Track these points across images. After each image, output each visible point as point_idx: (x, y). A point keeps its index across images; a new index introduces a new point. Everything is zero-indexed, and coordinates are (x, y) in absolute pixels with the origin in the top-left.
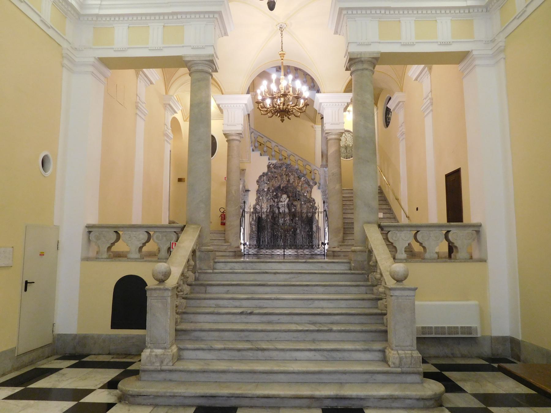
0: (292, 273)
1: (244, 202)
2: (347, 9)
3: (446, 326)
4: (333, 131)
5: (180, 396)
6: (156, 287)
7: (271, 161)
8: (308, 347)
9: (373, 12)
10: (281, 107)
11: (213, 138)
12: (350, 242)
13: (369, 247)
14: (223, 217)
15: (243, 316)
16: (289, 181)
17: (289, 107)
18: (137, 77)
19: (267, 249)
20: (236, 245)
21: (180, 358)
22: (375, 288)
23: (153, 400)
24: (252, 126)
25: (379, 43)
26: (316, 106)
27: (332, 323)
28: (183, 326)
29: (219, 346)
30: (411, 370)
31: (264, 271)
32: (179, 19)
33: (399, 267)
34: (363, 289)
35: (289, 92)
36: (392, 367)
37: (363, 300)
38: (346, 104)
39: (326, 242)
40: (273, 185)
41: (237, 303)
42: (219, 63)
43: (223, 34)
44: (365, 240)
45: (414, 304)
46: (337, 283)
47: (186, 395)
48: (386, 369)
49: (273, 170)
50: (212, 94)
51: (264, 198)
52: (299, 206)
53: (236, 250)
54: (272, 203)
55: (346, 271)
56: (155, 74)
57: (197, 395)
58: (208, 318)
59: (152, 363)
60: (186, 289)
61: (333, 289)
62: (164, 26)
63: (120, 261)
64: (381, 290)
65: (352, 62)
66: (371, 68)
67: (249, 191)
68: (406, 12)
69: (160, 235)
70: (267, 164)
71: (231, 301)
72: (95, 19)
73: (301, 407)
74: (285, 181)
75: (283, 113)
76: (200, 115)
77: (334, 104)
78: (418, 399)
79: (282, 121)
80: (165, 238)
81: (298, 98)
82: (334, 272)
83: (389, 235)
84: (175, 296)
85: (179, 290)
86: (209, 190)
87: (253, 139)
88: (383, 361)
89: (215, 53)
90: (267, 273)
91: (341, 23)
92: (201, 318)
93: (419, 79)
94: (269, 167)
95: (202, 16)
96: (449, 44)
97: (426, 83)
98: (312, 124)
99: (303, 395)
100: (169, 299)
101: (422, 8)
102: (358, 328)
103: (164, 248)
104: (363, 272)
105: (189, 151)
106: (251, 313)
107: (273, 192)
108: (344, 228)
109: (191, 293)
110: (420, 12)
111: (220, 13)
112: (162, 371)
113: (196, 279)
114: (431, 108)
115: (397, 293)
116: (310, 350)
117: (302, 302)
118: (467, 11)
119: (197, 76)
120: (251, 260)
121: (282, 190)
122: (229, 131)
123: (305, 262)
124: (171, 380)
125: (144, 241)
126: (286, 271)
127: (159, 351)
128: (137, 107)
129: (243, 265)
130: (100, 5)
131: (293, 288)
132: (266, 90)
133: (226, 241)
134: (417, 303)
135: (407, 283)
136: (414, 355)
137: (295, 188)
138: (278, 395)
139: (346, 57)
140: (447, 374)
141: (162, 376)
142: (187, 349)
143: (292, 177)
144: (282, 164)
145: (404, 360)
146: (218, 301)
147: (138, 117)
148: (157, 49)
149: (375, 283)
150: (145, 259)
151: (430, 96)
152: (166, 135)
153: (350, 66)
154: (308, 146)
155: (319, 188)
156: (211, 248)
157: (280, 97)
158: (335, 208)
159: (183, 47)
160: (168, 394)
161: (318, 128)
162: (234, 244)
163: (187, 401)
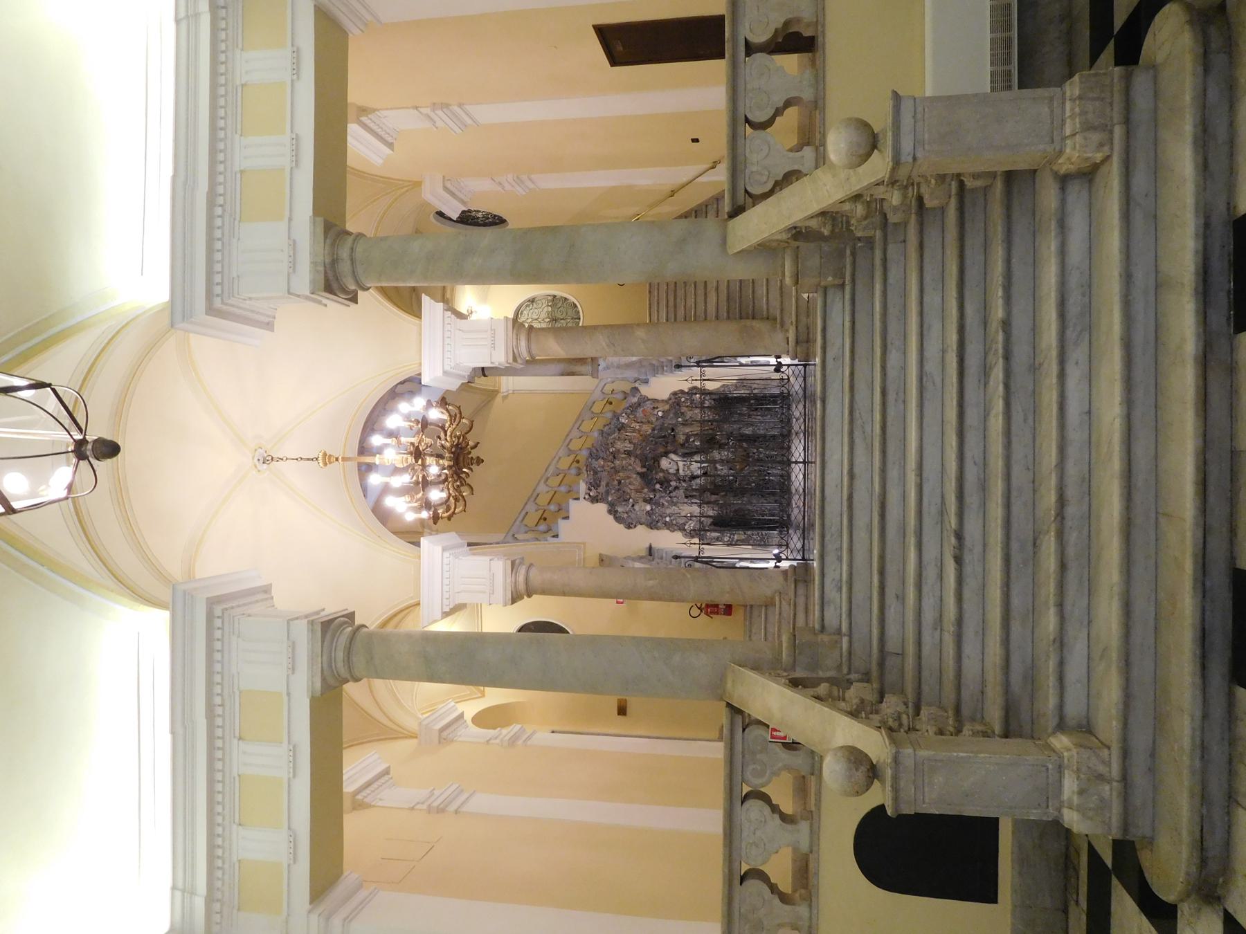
0: (851, 433)
1: (676, 557)
2: (209, 295)
3: (988, 36)
4: (510, 344)
5: (1203, 729)
6: (889, 788)
7: (582, 495)
8: (1054, 381)
9: (218, 234)
10: (446, 463)
11: (523, 629)
12: (775, 303)
13: (784, 236)
14: (711, 609)
15: (967, 558)
16: (629, 453)
17: (448, 445)
18: (369, 806)
19: (789, 504)
20: (781, 579)
21: (1085, 728)
22: (893, 218)
23: (1217, 806)
24: (500, 537)
25: (290, 219)
26: (454, 385)
27: (985, 324)
28: (994, 714)
29: (1050, 621)
30: (1118, 97)
31: (845, 503)
32: (223, 700)
33: (837, 144)
34: (892, 249)
35: (412, 444)
36: (1112, 149)
37: (921, 246)
38: (449, 313)
39: (773, 361)
40: (637, 491)
41: (930, 573)
42: (332, 607)
43: (265, 596)
44: (766, 249)
45: (933, 100)
46: (877, 317)
47: (1198, 714)
48: (1115, 166)
49: (602, 489)
50: (419, 629)
51: (668, 511)
52: (687, 430)
53: (791, 579)
54: (681, 492)
55: (847, 297)
56: (357, 768)
57: (1198, 681)
58: (970, 649)
59: (1103, 805)
60: (892, 705)
61: (893, 327)
62: (240, 739)
63: (817, 874)
64: (895, 198)
65: (335, 286)
66: (350, 239)
67: (650, 548)
68: (221, 157)
69: (751, 767)
70: (588, 504)
71: (925, 589)
72: (217, 907)
73: (1232, 393)
74: (631, 461)
75: (461, 458)
76: (463, 660)
77: (447, 341)
78: (1207, 70)
79: (480, 461)
80: (758, 756)
81: (424, 424)
82: (847, 324)
83: (756, 190)
84: (913, 735)
85: (895, 725)
86: (638, 641)
87: (530, 535)
88: (1091, 181)
89: (306, 617)
90: (850, 497)
91: (245, 313)
92: (971, 668)
93: (390, 139)
94: (594, 500)
95: (218, 645)
96: (297, 53)
97: (398, 120)
98: (499, 399)
99: (1197, 387)
100: (923, 753)
101: (213, 118)
102: (998, 253)
103: (784, 755)
104: (848, 252)
105: (542, 689)
106: (959, 536)
107: (654, 490)
108: (741, 318)
109: (902, 692)
110: (221, 123)
111: (212, 602)
112: (1125, 778)
113: (866, 677)
114: (456, 108)
115: (907, 145)
116: (1062, 375)
117: (926, 404)
118: (223, 13)
119: (359, 661)
120: (817, 538)
121: (650, 469)
122: (505, 590)
123: (824, 401)
124: (1153, 755)
125: (767, 810)
126: (846, 449)
127: (1070, 785)
128: (441, 810)
129: (830, 558)
130: (183, 891)
131: (890, 429)
132: (407, 498)
133: (769, 604)
134: (928, 93)
135: (880, 120)
136: (1077, 92)
137: (645, 438)
138: (1197, 455)
139: (325, 301)
140: (1119, 21)
141: (1139, 778)
142: (1061, 706)
143: (619, 445)
144: (589, 467)
145: (1090, 116)
146: (924, 623)
147: (464, 809)
148: (294, 760)
149: (877, 219)
150: (813, 808)
151: (427, 111)
152: (513, 741)
153: (345, 291)
154: (543, 401)
155: (646, 382)
156: (785, 638)
157: (424, 466)
158: (692, 339)
159: (289, 694)
160: (1198, 763)
161: (508, 383)
162: (778, 583)
163: (1218, 711)
